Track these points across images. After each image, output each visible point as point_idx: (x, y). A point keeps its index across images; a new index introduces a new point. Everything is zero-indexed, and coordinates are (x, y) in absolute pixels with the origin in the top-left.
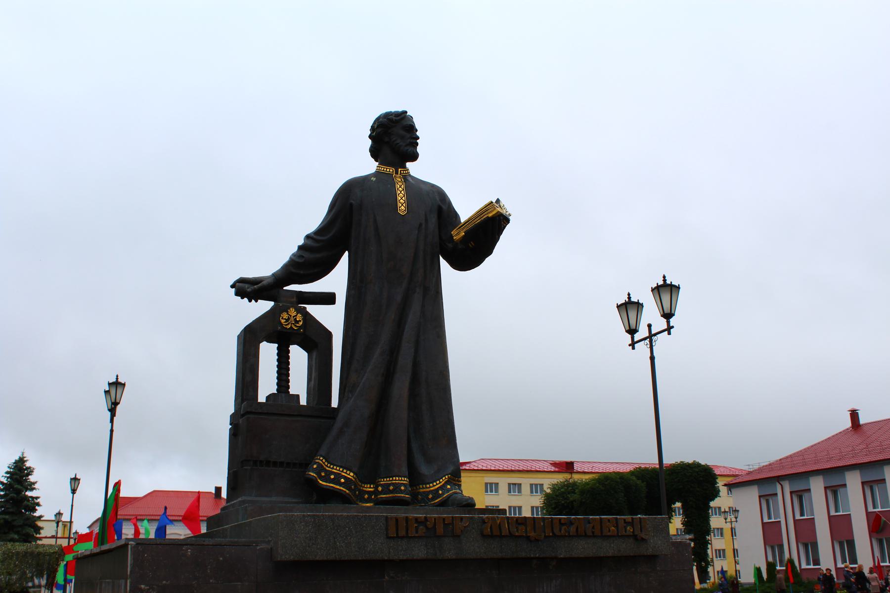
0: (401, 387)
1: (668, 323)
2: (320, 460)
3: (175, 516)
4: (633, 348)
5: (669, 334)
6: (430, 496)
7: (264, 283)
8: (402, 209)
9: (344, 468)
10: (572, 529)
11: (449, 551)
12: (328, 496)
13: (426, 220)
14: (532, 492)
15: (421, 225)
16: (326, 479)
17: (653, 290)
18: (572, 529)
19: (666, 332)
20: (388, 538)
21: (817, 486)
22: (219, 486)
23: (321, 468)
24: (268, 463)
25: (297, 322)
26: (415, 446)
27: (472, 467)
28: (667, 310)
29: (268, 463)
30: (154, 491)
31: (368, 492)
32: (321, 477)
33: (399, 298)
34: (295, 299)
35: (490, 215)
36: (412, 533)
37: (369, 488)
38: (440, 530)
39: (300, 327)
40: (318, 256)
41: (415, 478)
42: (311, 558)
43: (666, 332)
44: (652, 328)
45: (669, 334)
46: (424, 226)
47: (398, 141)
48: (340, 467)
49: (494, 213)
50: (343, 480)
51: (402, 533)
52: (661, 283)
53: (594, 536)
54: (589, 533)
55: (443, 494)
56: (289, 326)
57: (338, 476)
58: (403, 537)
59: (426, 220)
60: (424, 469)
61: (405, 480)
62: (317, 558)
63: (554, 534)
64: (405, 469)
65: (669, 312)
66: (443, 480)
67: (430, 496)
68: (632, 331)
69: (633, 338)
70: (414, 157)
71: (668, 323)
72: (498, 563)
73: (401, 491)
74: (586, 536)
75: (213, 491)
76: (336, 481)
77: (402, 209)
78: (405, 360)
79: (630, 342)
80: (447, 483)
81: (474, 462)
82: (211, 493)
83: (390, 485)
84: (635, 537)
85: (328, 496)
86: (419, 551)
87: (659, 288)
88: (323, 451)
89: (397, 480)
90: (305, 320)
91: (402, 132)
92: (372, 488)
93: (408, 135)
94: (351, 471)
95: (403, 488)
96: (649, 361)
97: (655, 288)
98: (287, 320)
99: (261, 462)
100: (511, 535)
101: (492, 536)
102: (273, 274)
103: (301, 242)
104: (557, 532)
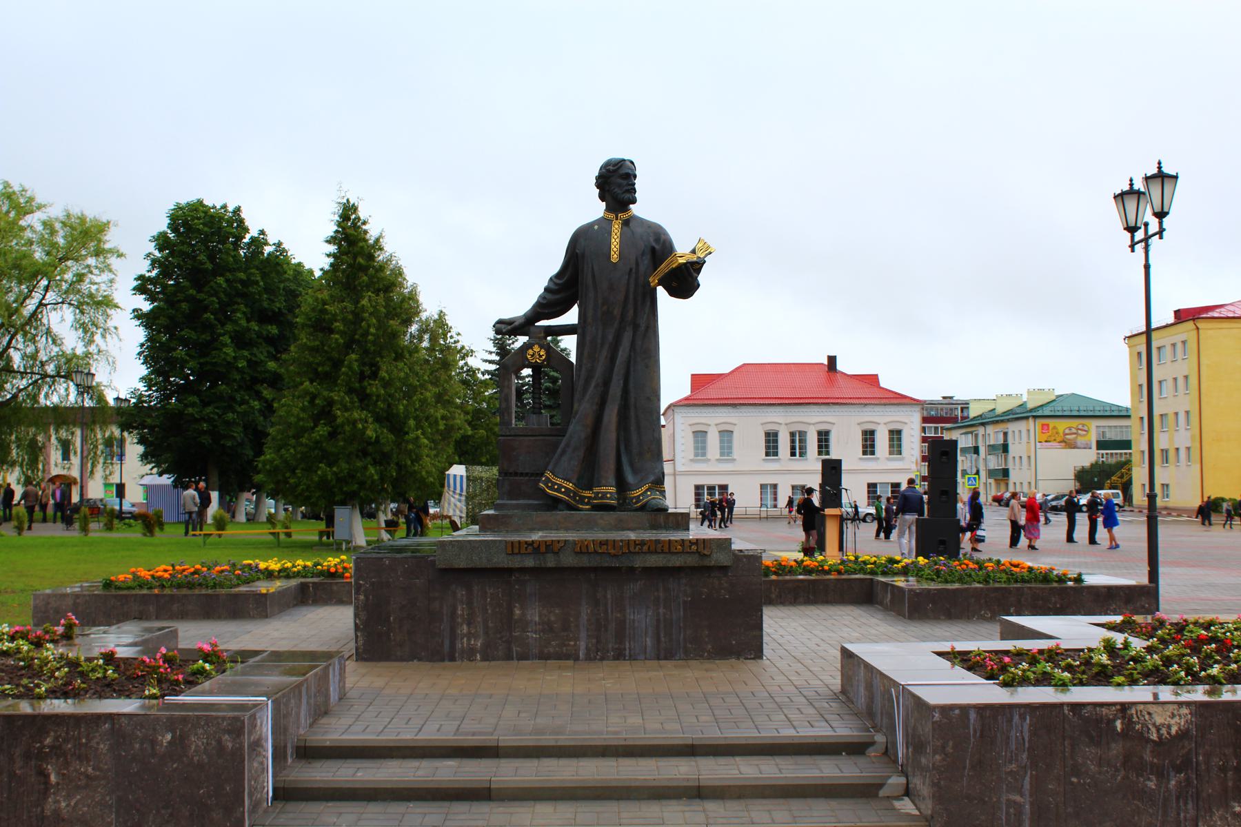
0: (611, 416)
1: (1161, 224)
2: (548, 474)
3: (771, 398)
4: (1133, 251)
5: (1161, 238)
6: (634, 501)
7: (516, 324)
8: (615, 257)
9: (565, 480)
10: (645, 548)
11: (551, 562)
12: (554, 504)
13: (637, 264)
14: (793, 454)
15: (631, 270)
16: (552, 488)
17: (1115, 197)
18: (645, 548)
19: (1158, 236)
20: (507, 554)
21: (659, 550)
22: (832, 354)
23: (548, 480)
24: (516, 474)
25: (541, 356)
26: (624, 460)
27: (1216, 314)
28: (1132, 223)
29: (516, 474)
30: (745, 365)
31: (589, 497)
32: (548, 487)
33: (610, 337)
34: (542, 335)
35: (674, 266)
36: (523, 551)
37: (587, 494)
38: (543, 549)
39: (544, 360)
40: (557, 297)
41: (622, 486)
42: (456, 566)
43: (1157, 236)
44: (1149, 227)
45: (1161, 238)
46: (634, 270)
47: (616, 190)
48: (562, 479)
49: (676, 264)
50: (563, 490)
51: (516, 551)
52: (1127, 188)
53: (662, 552)
54: (659, 550)
55: (643, 499)
56: (533, 361)
57: (560, 486)
58: (517, 554)
59: (637, 264)
60: (630, 478)
61: (613, 490)
62: (461, 567)
63: (630, 552)
64: (612, 480)
65: (1160, 210)
66: (644, 489)
67: (634, 501)
68: (1132, 230)
69: (1132, 238)
70: (634, 201)
71: (1161, 224)
72: (595, 570)
73: (608, 499)
74: (656, 552)
75: (826, 362)
76: (558, 490)
77: (615, 257)
78: (616, 390)
79: (1129, 243)
80: (647, 490)
81: (1231, 304)
82: (822, 364)
83: (599, 493)
84: (697, 552)
85: (554, 504)
86: (530, 562)
87: (1125, 196)
88: (550, 467)
89: (604, 489)
90: (548, 353)
91: (620, 181)
92: (97, 646)
93: (625, 182)
94: (570, 482)
95: (608, 496)
96: (1143, 270)
97: (1119, 195)
98: (532, 356)
99: (511, 473)
100: (596, 552)
101: (581, 552)
102: (524, 315)
103: (546, 284)
104: (632, 549)
